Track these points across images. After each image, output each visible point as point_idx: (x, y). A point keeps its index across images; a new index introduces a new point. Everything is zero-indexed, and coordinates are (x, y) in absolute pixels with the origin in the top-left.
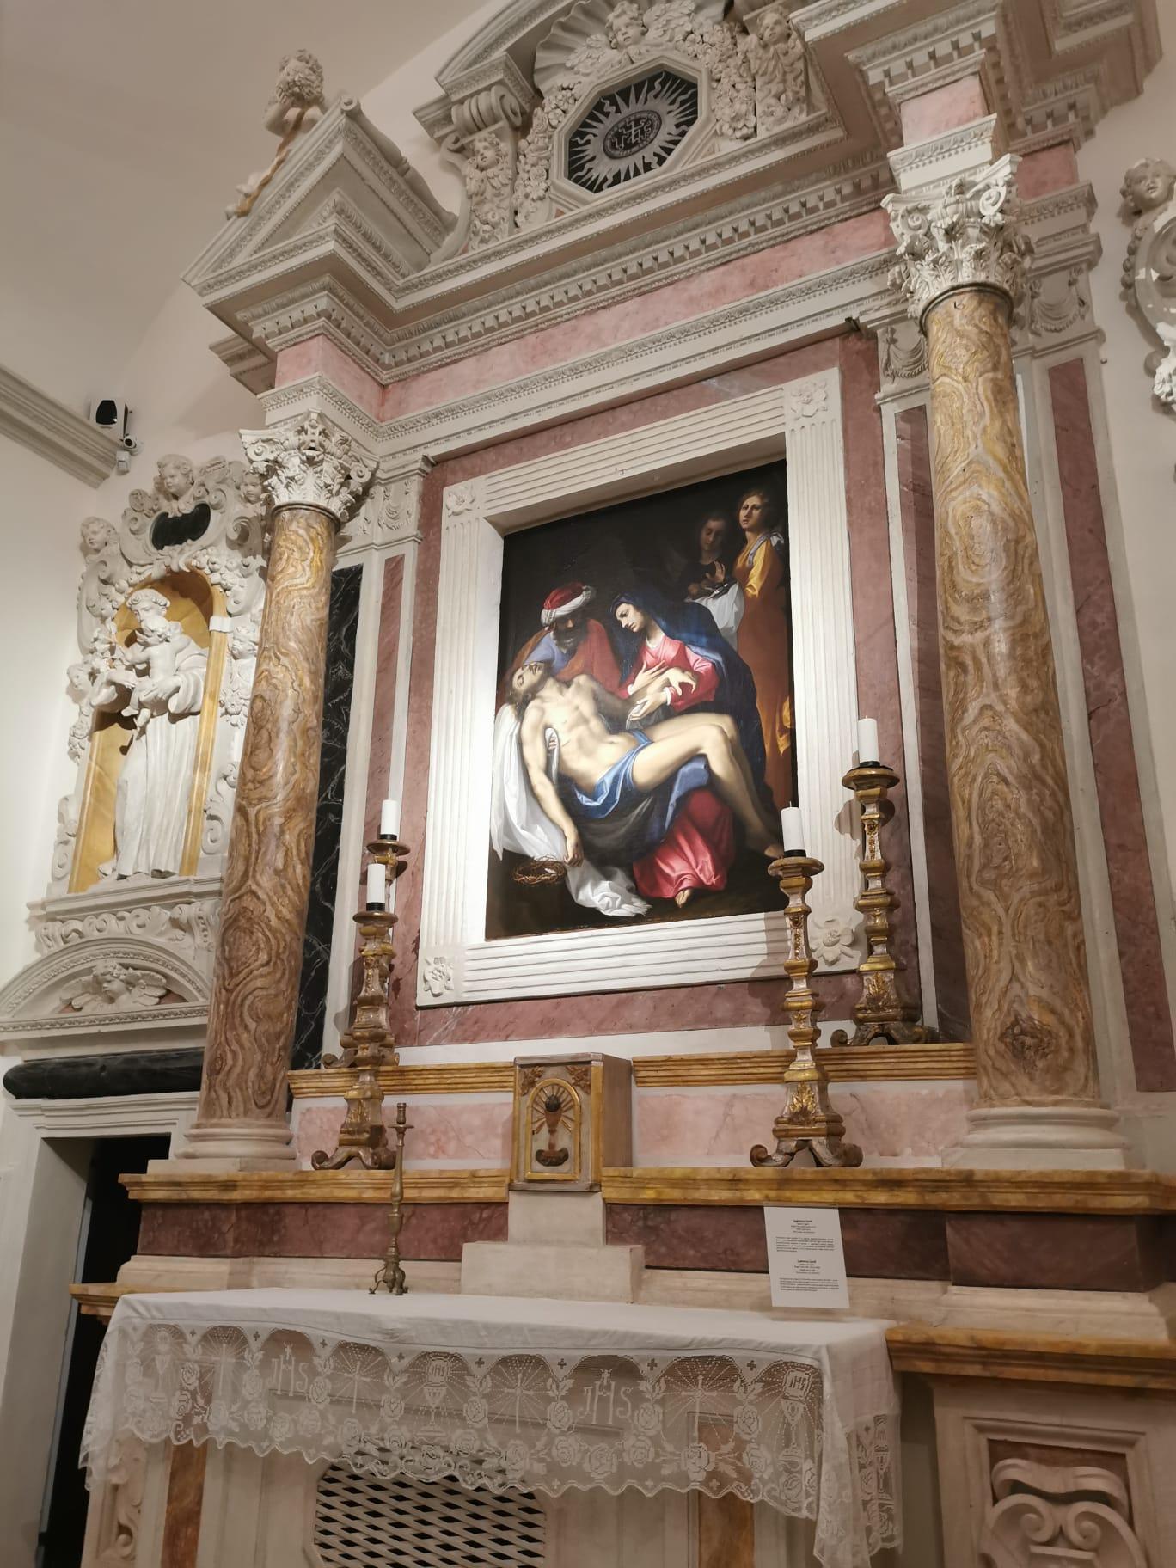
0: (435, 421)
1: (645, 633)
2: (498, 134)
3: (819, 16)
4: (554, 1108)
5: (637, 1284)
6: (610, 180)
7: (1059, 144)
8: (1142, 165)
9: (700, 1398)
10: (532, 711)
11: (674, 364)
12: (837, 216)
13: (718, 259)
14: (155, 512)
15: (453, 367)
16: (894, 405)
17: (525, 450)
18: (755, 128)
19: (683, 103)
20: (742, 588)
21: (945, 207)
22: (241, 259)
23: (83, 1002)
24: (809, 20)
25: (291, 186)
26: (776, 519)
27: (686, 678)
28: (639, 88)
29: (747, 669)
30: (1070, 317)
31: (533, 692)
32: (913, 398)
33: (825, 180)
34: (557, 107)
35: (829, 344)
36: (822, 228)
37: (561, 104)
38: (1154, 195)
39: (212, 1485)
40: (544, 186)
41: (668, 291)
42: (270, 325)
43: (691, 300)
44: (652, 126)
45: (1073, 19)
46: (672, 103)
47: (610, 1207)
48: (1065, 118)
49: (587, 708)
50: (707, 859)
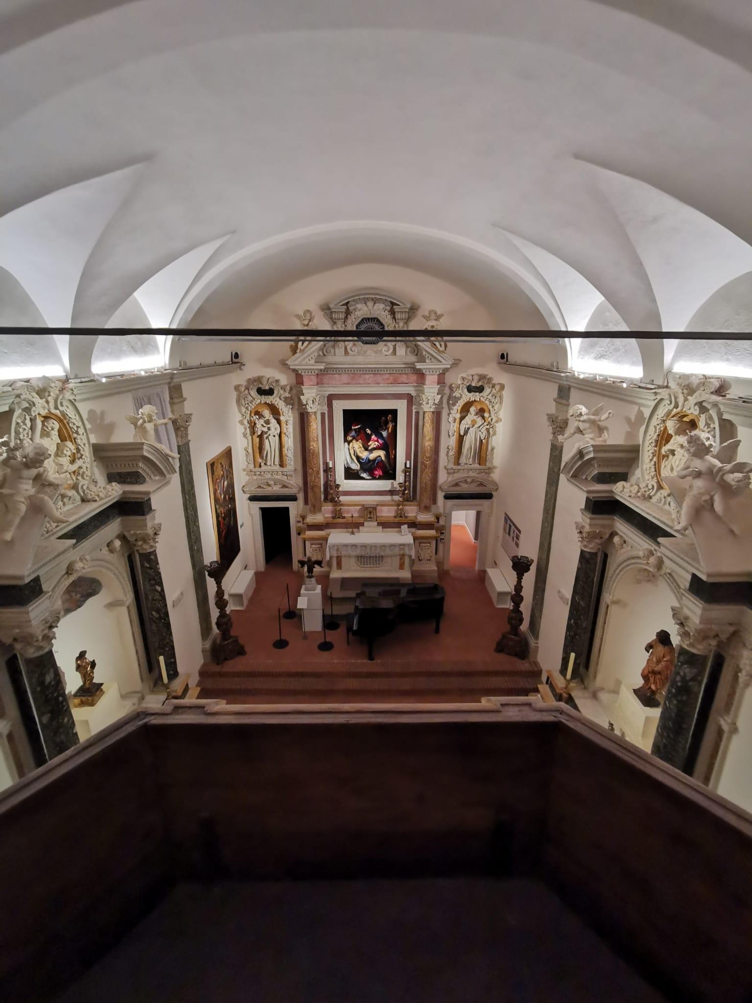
1: (371, 435)
4: (370, 513)
5: (383, 531)
9: (402, 547)
10: (351, 444)
20: (388, 430)
22: (296, 362)
25: (311, 348)
26: (395, 420)
27: (378, 444)
29: (388, 444)
31: (351, 441)
39: (343, 559)
41: (379, 375)
47: (378, 523)
49: (361, 446)
50: (381, 472)
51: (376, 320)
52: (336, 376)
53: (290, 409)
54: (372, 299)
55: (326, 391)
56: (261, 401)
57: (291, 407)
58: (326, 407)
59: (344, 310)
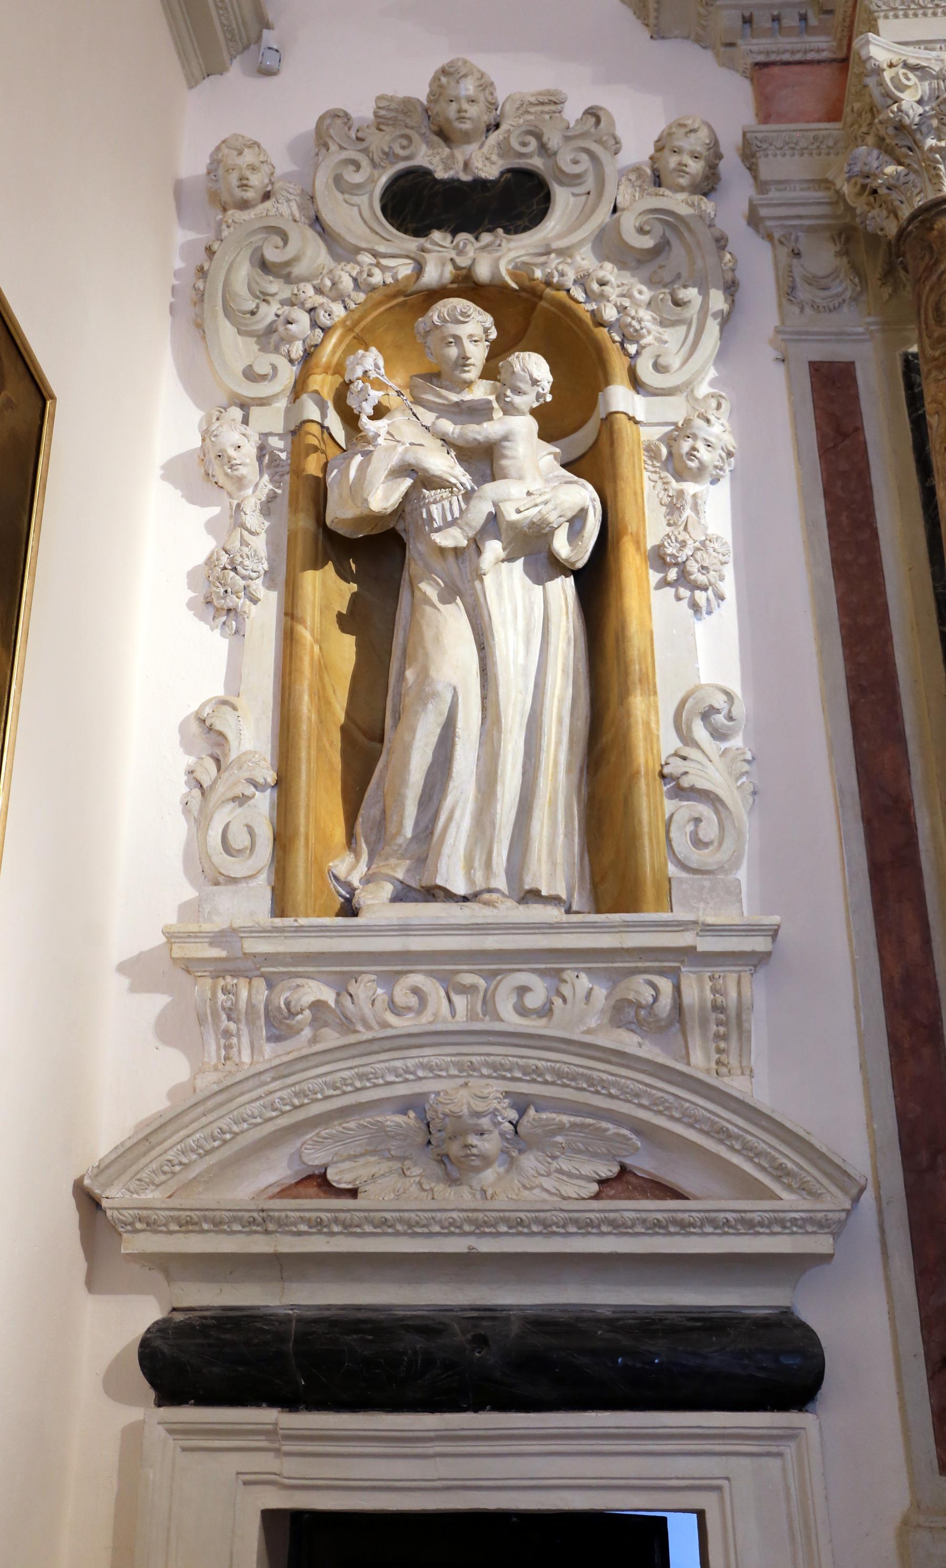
14: (398, 158)
23: (365, 1173)
53: (713, 328)
56: (420, 269)
57: (718, 300)
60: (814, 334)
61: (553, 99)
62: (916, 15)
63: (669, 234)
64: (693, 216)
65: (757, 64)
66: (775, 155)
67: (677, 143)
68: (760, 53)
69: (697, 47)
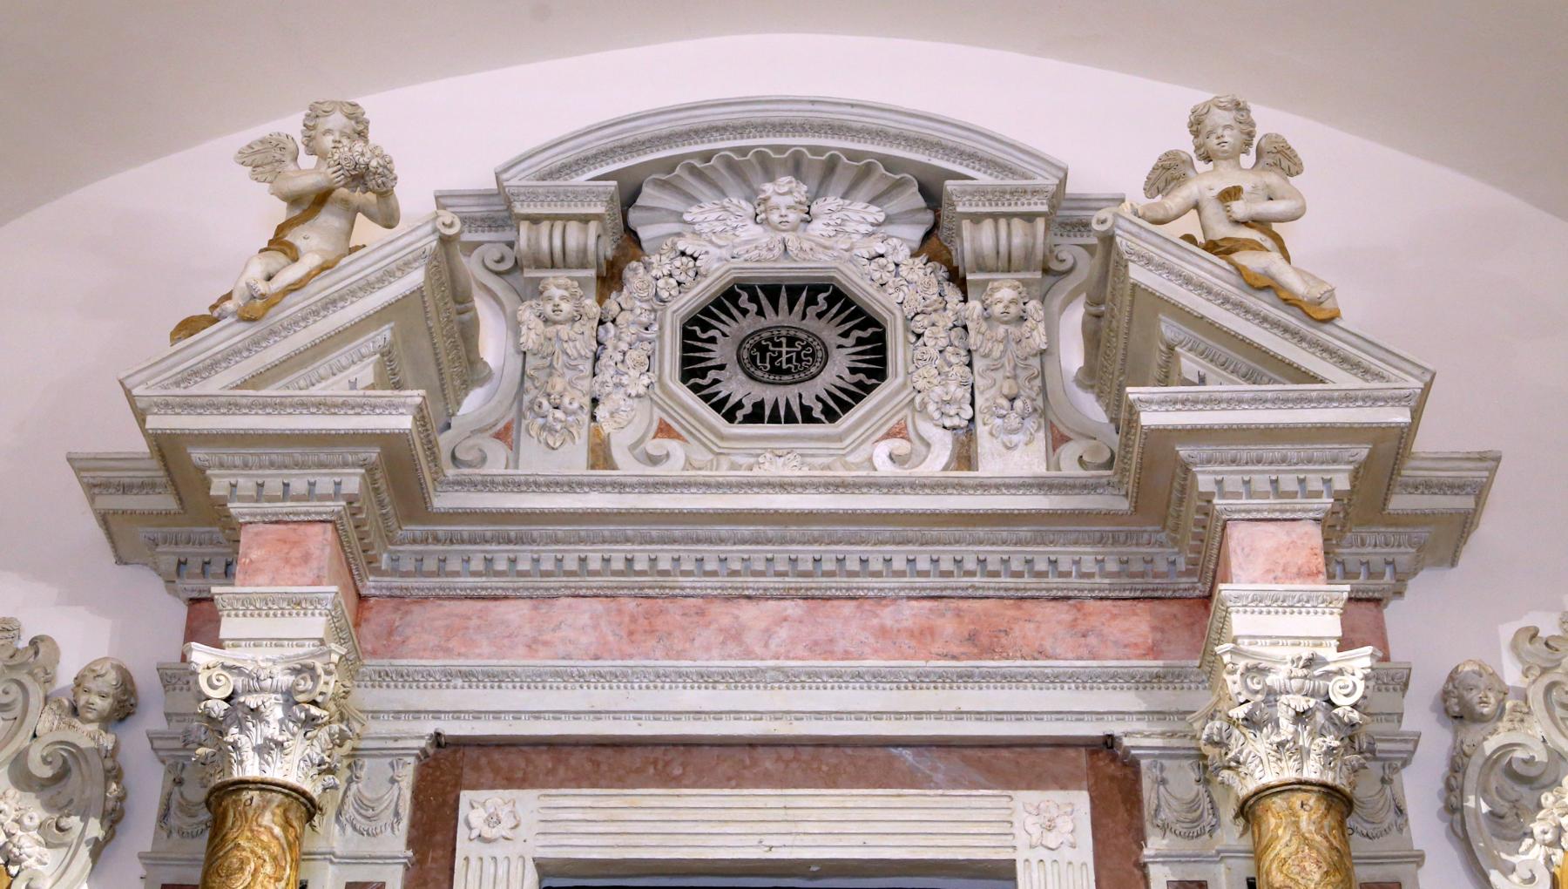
0: (459, 682)
2: (582, 283)
3: (1161, 402)
6: (748, 409)
7: (1368, 600)
8: (1474, 672)
11: (858, 715)
12: (1093, 590)
13: (924, 589)
15: (491, 604)
16: (1166, 869)
17: (604, 768)
18: (972, 420)
19: (860, 341)
21: (1290, 678)
22: (216, 385)
24: (1150, 402)
25: (331, 303)
28: (794, 291)
30: (1385, 825)
32: (1191, 867)
33: (1087, 544)
34: (671, 276)
35: (1071, 753)
36: (1069, 598)
37: (676, 273)
38: (1486, 710)
40: (646, 381)
41: (848, 608)
42: (246, 484)
43: (883, 632)
44: (813, 355)
45: (1411, 481)
46: (845, 335)
48: (1382, 575)
51: (821, 297)
52: (514, 613)
53: (84, 853)
54: (797, 165)
55: (417, 714)
57: (95, 829)
58: (395, 841)
59: (600, 209)
60: (172, 859)
61: (7, 627)
62: (252, 615)
63: (70, 761)
64: (92, 749)
65: (191, 599)
66: (182, 689)
67: (87, 685)
68: (193, 591)
69: (153, 573)
